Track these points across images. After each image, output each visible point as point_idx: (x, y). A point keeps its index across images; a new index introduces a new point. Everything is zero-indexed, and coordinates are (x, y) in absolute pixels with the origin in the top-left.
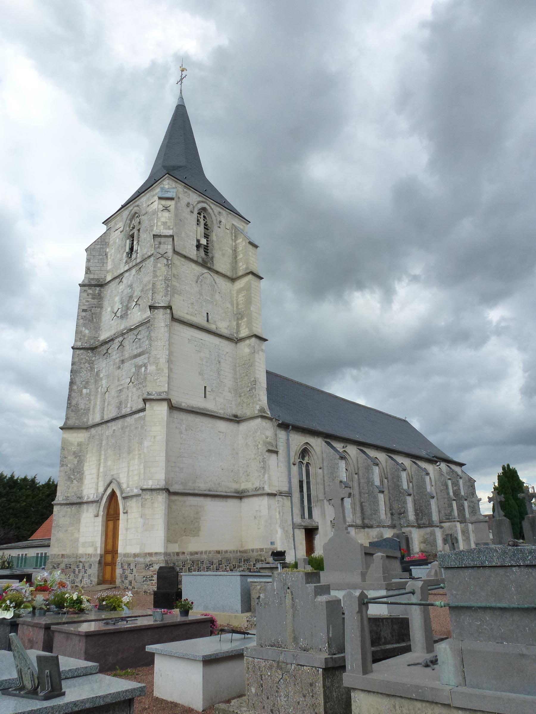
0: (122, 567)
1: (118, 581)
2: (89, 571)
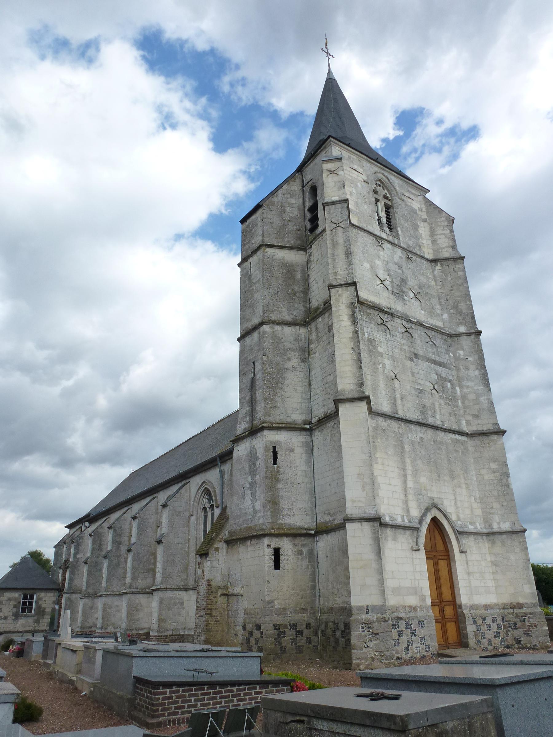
0: (475, 622)
1: (472, 642)
2: (421, 632)
